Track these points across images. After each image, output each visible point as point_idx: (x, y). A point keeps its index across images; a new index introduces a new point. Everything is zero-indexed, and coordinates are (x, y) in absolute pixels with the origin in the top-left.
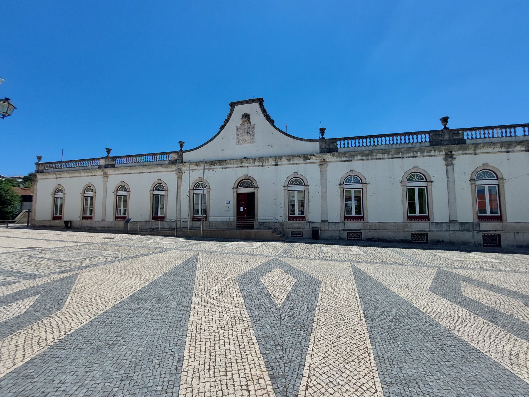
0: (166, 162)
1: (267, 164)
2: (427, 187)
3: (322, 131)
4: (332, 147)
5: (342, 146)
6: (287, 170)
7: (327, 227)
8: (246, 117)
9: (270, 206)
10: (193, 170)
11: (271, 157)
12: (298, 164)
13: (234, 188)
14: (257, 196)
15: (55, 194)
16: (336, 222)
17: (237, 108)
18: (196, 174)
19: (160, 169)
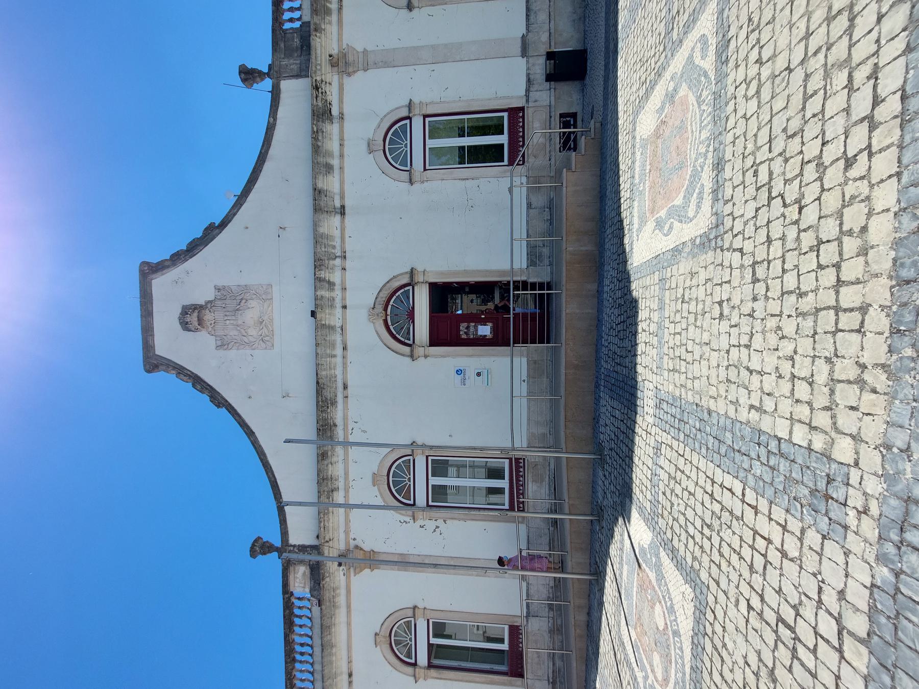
0: (316, 610)
1: (337, 243)
2: (425, 116)
3: (249, 75)
4: (297, 41)
5: (296, 15)
6: (360, 174)
7: (544, 37)
8: (192, 316)
9: (477, 227)
10: (346, 436)
11: (315, 225)
12: (342, 139)
13: (412, 356)
14: (442, 273)
15: (415, 665)
16: (528, 9)
17: (162, 349)
18: (359, 473)
19: (340, 634)
